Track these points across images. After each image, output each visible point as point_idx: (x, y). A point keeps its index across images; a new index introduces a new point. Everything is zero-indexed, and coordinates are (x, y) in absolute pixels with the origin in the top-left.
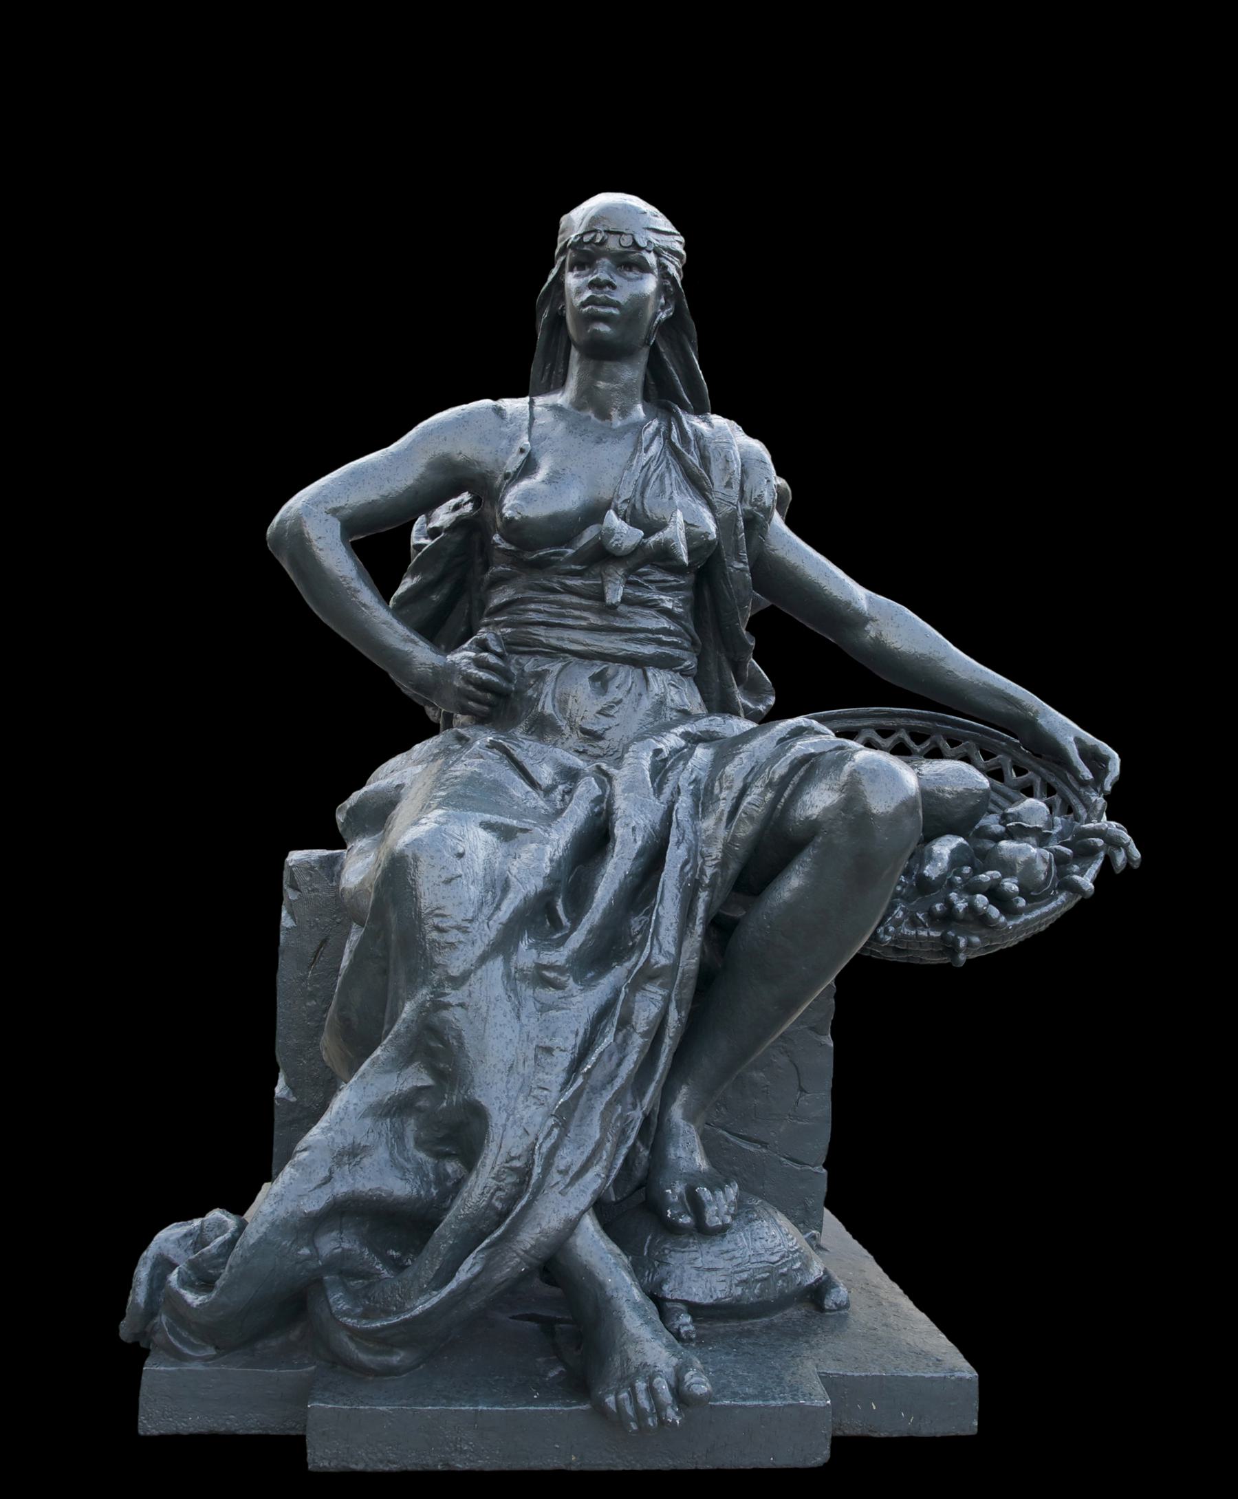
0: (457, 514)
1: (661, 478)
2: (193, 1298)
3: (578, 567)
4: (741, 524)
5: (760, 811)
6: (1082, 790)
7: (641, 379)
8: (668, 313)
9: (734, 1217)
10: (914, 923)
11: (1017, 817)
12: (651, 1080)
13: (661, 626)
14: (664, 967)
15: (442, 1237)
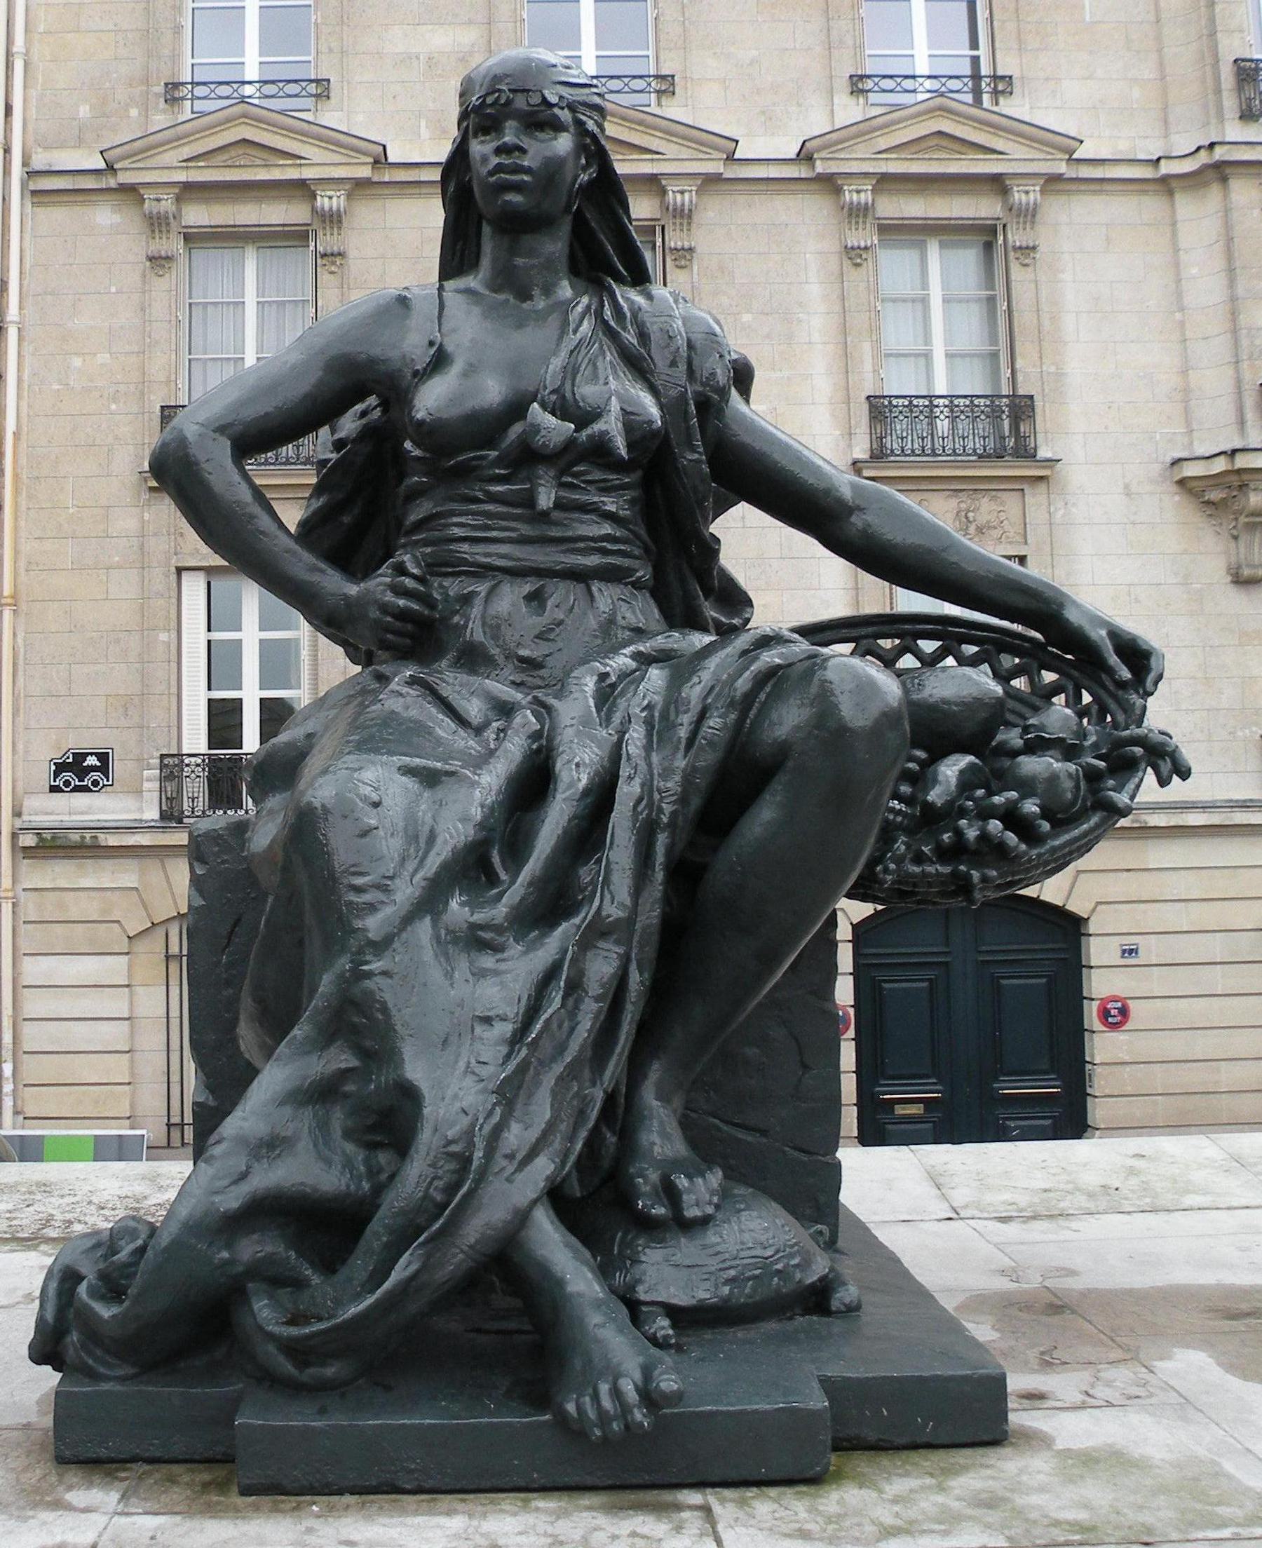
0: (364, 421)
1: (593, 363)
2: (106, 1312)
6: (1120, 693)
7: (566, 251)
8: (590, 175)
9: (717, 1207)
10: (919, 859)
11: (1041, 728)
12: (612, 1052)
13: (603, 532)
14: (618, 920)
15: (376, 1233)
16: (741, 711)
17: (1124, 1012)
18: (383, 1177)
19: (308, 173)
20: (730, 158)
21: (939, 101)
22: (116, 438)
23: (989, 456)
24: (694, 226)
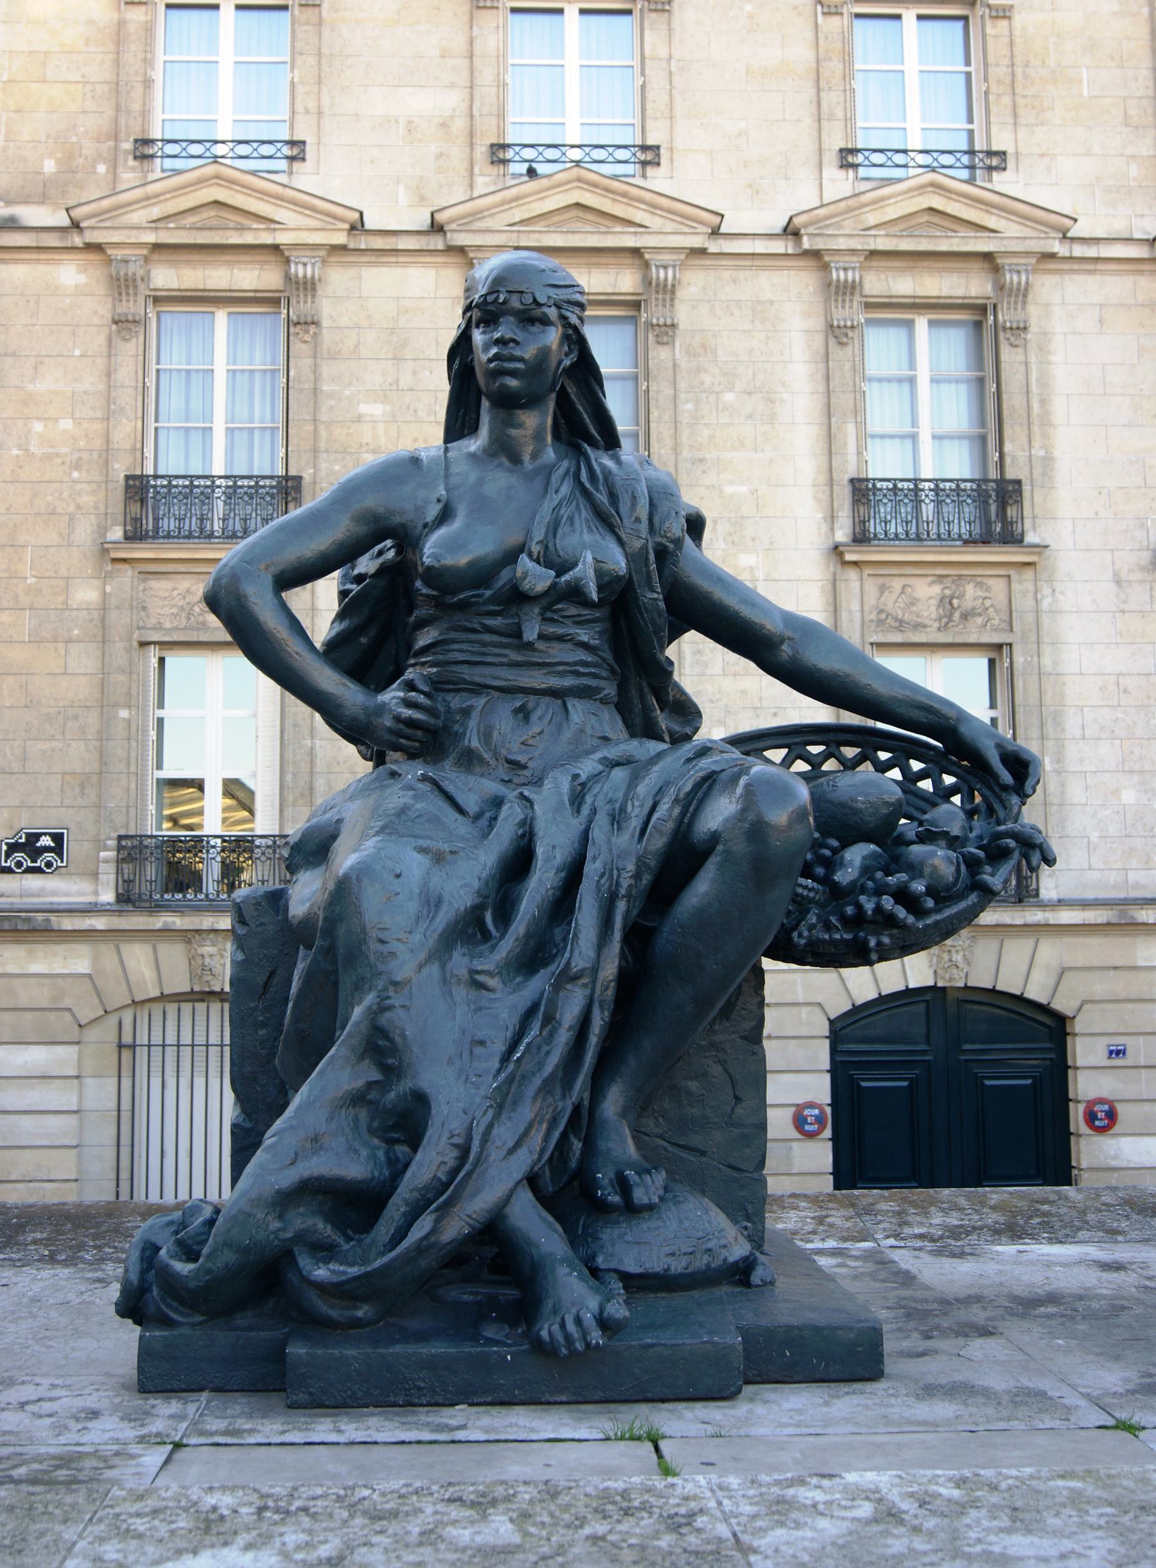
1: (571, 520)
2: (183, 1268)
3: (496, 608)
4: (652, 557)
5: (670, 825)
10: (828, 927)
11: (932, 822)
13: (577, 659)
16: (683, 807)
17: (1112, 1116)
18: (400, 1166)
19: (282, 238)
20: (715, 232)
21: (931, 177)
22: (79, 507)
23: (975, 542)
24: (677, 302)
